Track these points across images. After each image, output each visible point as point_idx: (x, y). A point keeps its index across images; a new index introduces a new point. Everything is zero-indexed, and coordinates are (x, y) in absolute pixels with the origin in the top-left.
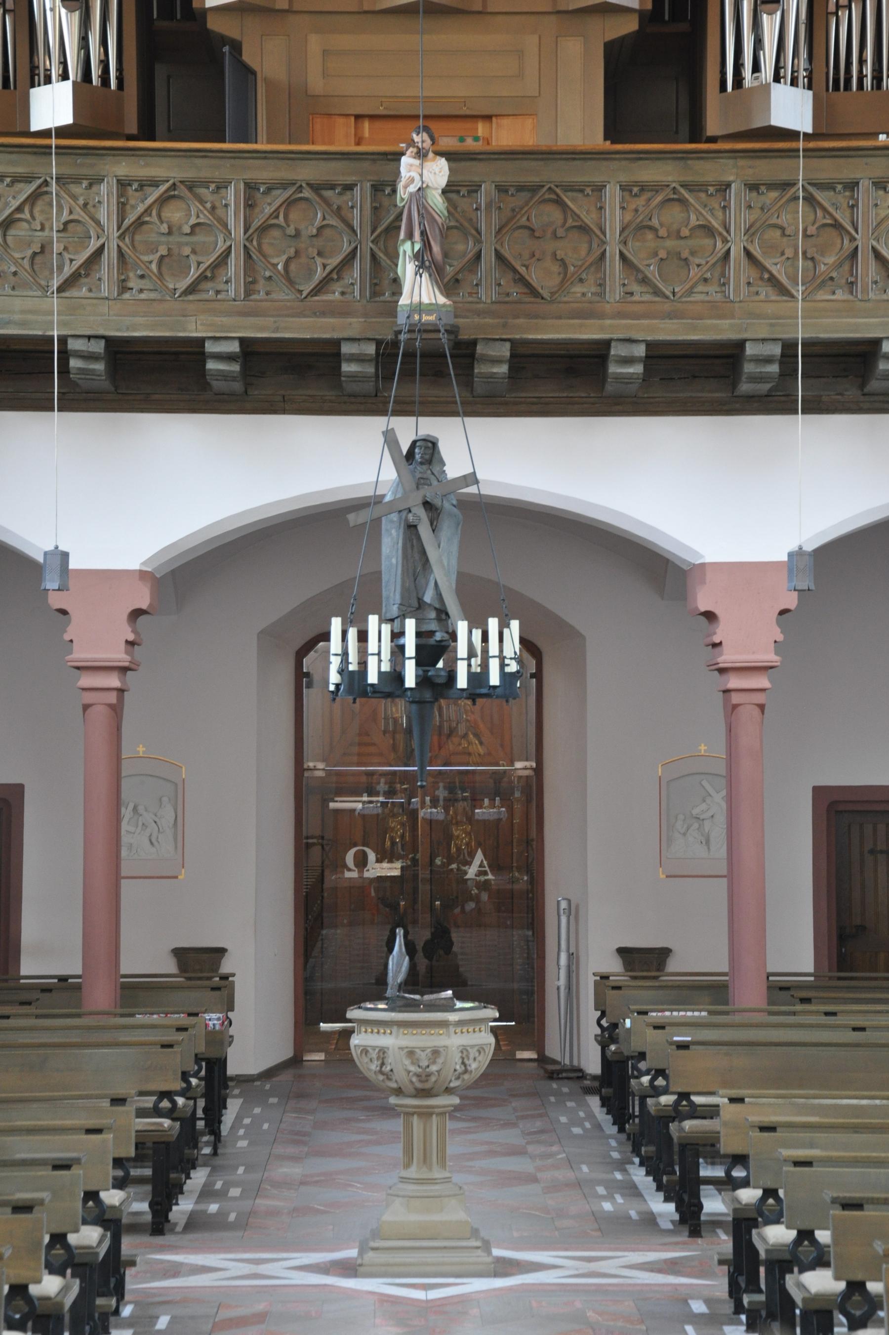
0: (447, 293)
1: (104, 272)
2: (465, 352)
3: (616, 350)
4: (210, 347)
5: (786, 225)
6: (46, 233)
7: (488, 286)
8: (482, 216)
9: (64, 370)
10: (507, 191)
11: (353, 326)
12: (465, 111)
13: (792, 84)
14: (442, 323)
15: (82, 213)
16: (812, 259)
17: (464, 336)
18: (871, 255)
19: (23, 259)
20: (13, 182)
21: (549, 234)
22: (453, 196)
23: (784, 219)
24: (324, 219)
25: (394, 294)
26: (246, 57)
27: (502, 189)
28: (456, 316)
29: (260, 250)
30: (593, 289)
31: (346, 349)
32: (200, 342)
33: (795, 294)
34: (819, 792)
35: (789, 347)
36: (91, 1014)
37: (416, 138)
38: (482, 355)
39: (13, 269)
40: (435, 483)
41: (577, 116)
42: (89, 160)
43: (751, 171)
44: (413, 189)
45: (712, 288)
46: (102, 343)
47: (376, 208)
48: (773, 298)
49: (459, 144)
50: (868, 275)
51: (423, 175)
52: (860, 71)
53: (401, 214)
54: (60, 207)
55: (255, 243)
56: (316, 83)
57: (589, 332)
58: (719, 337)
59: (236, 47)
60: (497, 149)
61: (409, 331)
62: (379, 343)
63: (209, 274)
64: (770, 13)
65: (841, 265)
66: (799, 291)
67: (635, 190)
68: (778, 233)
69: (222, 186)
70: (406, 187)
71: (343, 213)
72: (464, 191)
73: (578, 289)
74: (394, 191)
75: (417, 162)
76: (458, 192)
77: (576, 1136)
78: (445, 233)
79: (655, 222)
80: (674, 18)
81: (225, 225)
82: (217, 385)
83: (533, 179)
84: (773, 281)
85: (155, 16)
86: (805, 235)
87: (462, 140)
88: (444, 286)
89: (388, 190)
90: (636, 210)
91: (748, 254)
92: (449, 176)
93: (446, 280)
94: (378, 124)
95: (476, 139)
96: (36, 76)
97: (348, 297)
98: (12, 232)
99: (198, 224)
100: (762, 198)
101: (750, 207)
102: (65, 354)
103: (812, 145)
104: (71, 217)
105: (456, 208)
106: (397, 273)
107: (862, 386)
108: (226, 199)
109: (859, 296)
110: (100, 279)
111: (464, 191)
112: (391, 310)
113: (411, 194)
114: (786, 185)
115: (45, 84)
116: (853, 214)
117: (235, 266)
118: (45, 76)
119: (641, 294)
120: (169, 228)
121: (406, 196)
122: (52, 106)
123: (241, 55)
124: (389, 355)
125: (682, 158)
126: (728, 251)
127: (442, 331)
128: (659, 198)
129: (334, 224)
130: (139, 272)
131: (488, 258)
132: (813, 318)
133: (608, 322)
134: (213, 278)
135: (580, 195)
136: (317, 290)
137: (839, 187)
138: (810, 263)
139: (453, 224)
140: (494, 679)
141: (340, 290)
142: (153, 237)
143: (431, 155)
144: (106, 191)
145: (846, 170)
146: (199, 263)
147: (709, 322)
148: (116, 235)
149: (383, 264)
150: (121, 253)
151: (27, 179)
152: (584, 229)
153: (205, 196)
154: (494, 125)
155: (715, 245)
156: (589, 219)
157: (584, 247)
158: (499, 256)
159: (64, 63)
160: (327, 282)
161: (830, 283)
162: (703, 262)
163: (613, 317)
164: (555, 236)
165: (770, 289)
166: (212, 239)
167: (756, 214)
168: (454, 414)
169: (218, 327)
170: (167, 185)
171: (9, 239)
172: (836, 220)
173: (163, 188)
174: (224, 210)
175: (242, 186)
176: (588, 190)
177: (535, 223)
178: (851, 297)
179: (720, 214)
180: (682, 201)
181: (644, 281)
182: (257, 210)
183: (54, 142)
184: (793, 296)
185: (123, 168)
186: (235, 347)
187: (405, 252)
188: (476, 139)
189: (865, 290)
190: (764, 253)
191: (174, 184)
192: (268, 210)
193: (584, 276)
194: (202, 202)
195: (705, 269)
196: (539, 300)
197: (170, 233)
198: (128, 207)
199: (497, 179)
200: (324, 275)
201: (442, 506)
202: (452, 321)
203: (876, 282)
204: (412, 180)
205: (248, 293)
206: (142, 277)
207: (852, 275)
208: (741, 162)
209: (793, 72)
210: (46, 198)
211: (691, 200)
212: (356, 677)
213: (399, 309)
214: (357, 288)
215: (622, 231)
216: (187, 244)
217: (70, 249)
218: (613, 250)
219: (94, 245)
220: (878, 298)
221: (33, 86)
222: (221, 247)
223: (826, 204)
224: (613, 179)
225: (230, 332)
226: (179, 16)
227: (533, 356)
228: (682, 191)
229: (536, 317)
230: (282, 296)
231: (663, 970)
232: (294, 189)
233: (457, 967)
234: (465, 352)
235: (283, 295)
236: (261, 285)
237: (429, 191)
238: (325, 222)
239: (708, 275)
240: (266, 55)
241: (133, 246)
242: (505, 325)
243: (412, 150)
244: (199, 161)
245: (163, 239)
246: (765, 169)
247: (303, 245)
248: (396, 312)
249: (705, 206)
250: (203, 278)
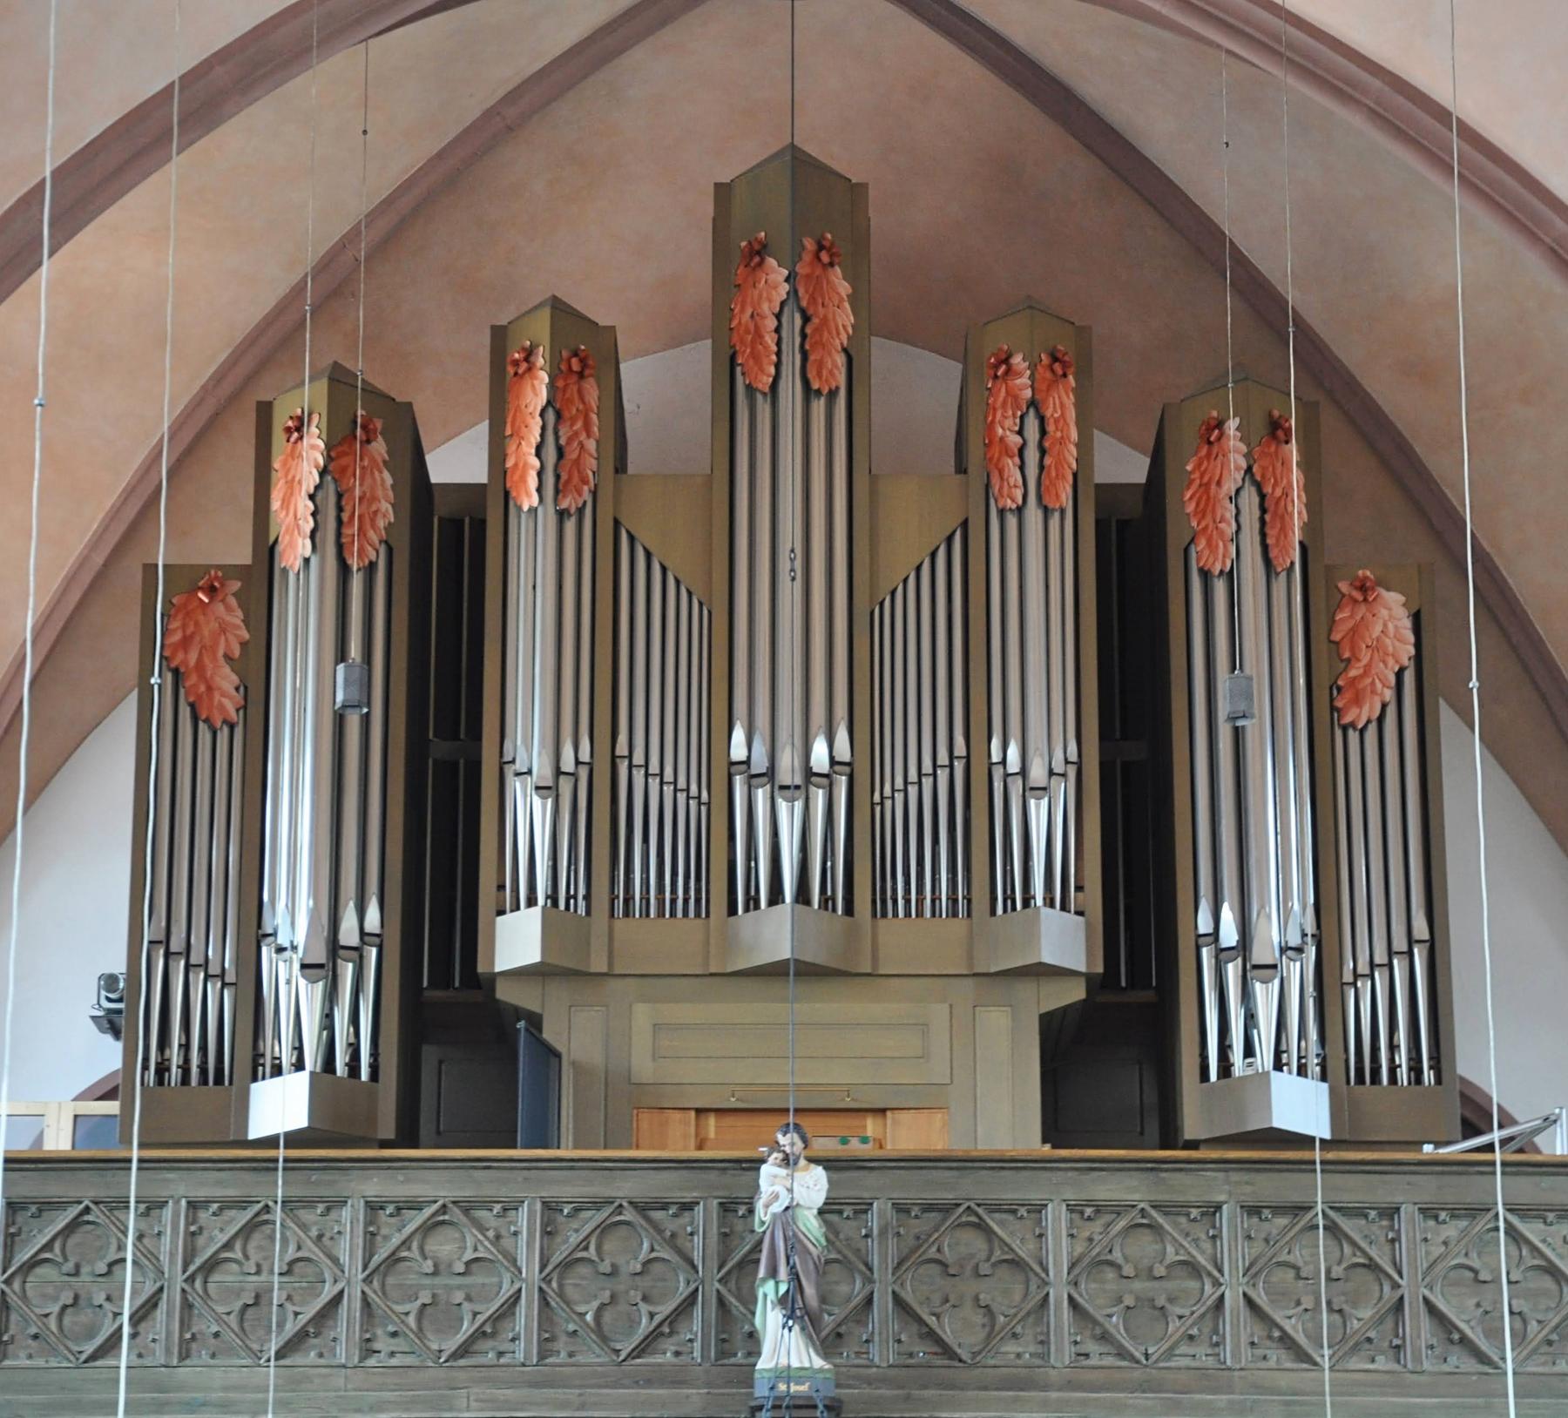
1: (342, 1329)
5: (1300, 1263)
6: (263, 1277)
7: (883, 1342)
8: (874, 1245)
10: (908, 1212)
12: (848, 1103)
13: (1299, 1074)
14: (821, 1394)
15: (316, 1250)
16: (1340, 1311)
19: (228, 1314)
20: (221, 1209)
21: (968, 1270)
22: (834, 1218)
23: (1297, 1257)
24: (652, 1250)
27: (901, 1209)
28: (838, 1386)
29: (561, 1294)
30: (1032, 1349)
33: (1318, 1359)
37: (783, 1140)
39: (214, 1328)
41: (1002, 1107)
43: (1248, 1189)
44: (777, 1208)
45: (1201, 1350)
47: (726, 1235)
48: (1289, 1365)
49: (840, 1147)
50: (1419, 1336)
51: (791, 1191)
52: (1392, 1060)
53: (760, 1242)
54: (285, 1240)
55: (554, 1285)
56: (643, 1066)
59: (535, 1021)
60: (894, 1155)
61: (775, 1407)
65: (1381, 1321)
67: (1089, 1211)
68: (1291, 1274)
69: (510, 1207)
70: (767, 1206)
71: (679, 1242)
72: (848, 1211)
73: (1011, 1348)
74: (751, 1211)
75: (783, 1172)
76: (840, 1212)
78: (823, 1268)
79: (1117, 1256)
80: (1132, 984)
81: (514, 1261)
84: (1286, 1341)
85: (425, 984)
86: (1329, 1279)
87: (845, 1141)
88: (823, 1342)
89: (742, 1211)
90: (1090, 1240)
91: (1250, 1302)
92: (829, 1191)
93: (824, 1334)
94: (729, 1121)
95: (864, 1140)
96: (259, 1066)
97: (684, 1359)
100: (1266, 1225)
101: (1249, 1237)
103: (1331, 1156)
104: (300, 1254)
105: (837, 1234)
106: (753, 1325)
108: (515, 1223)
109: (1410, 1366)
110: (335, 1340)
111: (848, 1211)
112: (746, 1376)
113: (774, 1215)
115: (272, 1076)
116: (1394, 1250)
117: (525, 1318)
118: (273, 1066)
119: (1098, 1355)
120: (435, 1265)
121: (767, 1219)
122: (280, 1105)
123: (540, 1031)
125: (1152, 1169)
127: (821, 1407)
128: (1122, 1223)
129: (666, 1256)
130: (391, 1328)
133: (1054, 1395)
134: (494, 1335)
135: (1010, 1217)
136: (640, 1350)
137: (1373, 1214)
138: (1337, 1317)
139: (833, 1256)
141: (673, 1348)
142: (412, 1279)
143: (802, 1162)
144: (350, 1217)
146: (475, 1314)
147: (1198, 1396)
148: (361, 1276)
149: (734, 1311)
150: (366, 1303)
151: (242, 1204)
152: (1016, 1263)
154: (889, 1121)
155: (1203, 1290)
156: (1024, 1251)
158: (898, 1301)
159: (299, 1049)
160: (655, 1339)
161: (1367, 1346)
162: (1187, 1312)
164: (977, 1274)
165: (1283, 1354)
166: (495, 1280)
167: (1258, 1247)
170: (435, 1207)
172: (1371, 1259)
173: (428, 1211)
174: (513, 1239)
175: (538, 1206)
176: (1023, 1211)
177: (948, 1255)
178: (1396, 1367)
179: (1207, 1246)
180: (1153, 1227)
181: (1105, 1337)
182: (559, 1239)
183: (281, 1153)
184: (1315, 1364)
185: (375, 1186)
187: (765, 1296)
188: (864, 1140)
189: (1417, 1359)
190: (1272, 1302)
191: (444, 1206)
192: (574, 1239)
193: (1018, 1329)
194: (483, 1230)
195: (1190, 1322)
196: (957, 1364)
197: (436, 1273)
198: (379, 1238)
199: (895, 1195)
202: (835, 1392)
203: (1432, 1347)
204: (776, 1197)
205: (542, 1356)
206: (394, 1334)
207: (1397, 1336)
208: (1235, 1177)
209: (1300, 1058)
210: (267, 1229)
211: (1167, 1227)
213: (757, 1375)
214: (697, 1345)
216: (459, 1287)
217: (296, 1298)
218: (1058, 1293)
220: (1436, 1369)
221: (255, 1079)
222: (507, 1290)
224: (1053, 1198)
225: (516, 1410)
226: (457, 984)
228: (1154, 1213)
229: (952, 1387)
230: (593, 1359)
232: (611, 1209)
235: (593, 1356)
236: (562, 1345)
237: (799, 1211)
238: (654, 1255)
239: (1194, 1331)
240: (575, 1032)
241: (384, 1293)
245: (427, 1281)
246: (1269, 1187)
247: (622, 1287)
248: (752, 1379)
249: (1187, 1235)
250: (480, 1334)
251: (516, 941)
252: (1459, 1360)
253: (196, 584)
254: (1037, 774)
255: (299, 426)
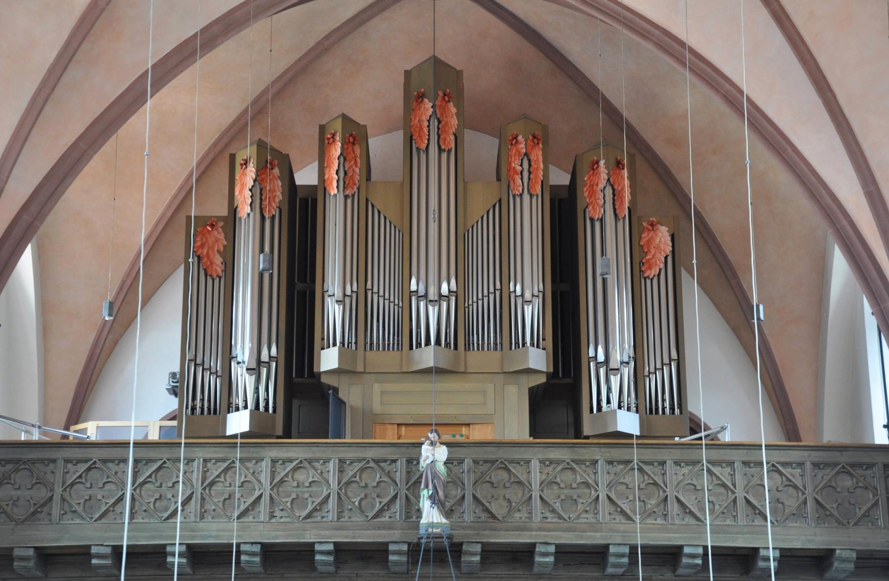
2: (457, 549)
4: (318, 547)
6: (232, 488)
7: (469, 513)
8: (465, 475)
9: (238, 562)
10: (478, 463)
11: (396, 535)
12: (456, 421)
16: (643, 501)
17: (455, 540)
18: (675, 500)
22: (450, 465)
23: (627, 480)
25: (418, 517)
26: (341, 395)
27: (476, 462)
28: (452, 529)
29: (346, 495)
31: (392, 547)
35: (633, 549)
41: (516, 425)
43: (608, 454)
44: (428, 461)
45: (590, 516)
46: (259, 546)
51: (433, 455)
52: (663, 405)
54: (240, 474)
56: (377, 408)
57: (524, 539)
58: (594, 542)
59: (336, 390)
60: (473, 441)
61: (428, 538)
62: (409, 544)
66: (637, 518)
67: (547, 463)
68: (624, 487)
69: (326, 461)
72: (455, 463)
73: (517, 515)
74: (418, 463)
75: (431, 448)
78: (446, 485)
79: (558, 480)
80: (564, 376)
81: (328, 482)
82: (320, 568)
84: (623, 512)
86: (639, 489)
87: (454, 436)
91: (609, 498)
94: (410, 428)
95: (462, 436)
96: (231, 407)
98: (214, 488)
99: (313, 481)
102: (239, 553)
103: (640, 442)
107: (674, 571)
111: (455, 463)
114: (628, 462)
117: (332, 503)
121: (425, 466)
122: (238, 423)
124: (416, 551)
126: (598, 496)
128: (560, 467)
131: (469, 498)
133: (534, 533)
134: (320, 510)
136: (376, 516)
142: (289, 489)
143: (438, 444)
144: (265, 465)
145: (660, 455)
150: (271, 498)
151: (223, 460)
152: (520, 483)
156: (523, 478)
158: (475, 497)
159: (246, 401)
164: (505, 487)
167: (612, 476)
171: (212, 492)
173: (295, 463)
176: (522, 463)
177: (494, 480)
179: (592, 476)
180: (572, 469)
181: (553, 511)
183: (239, 441)
185: (275, 453)
188: (462, 436)
189: (673, 519)
192: (351, 473)
194: (316, 470)
197: (298, 486)
202: (450, 532)
204: (428, 457)
205: (339, 518)
206: (282, 510)
208: (603, 450)
210: (233, 469)
214: (398, 514)
218: (536, 494)
219: (257, 493)
221: (229, 412)
222: (325, 493)
224: (535, 457)
229: (495, 530)
234: (457, 549)
235: (358, 518)
236: (346, 514)
239: (588, 509)
240: (351, 394)
242: (478, 534)
245: (295, 490)
246: (616, 454)
247: (368, 492)
251: (329, 360)
252: (689, 520)
253: (206, 223)
254: (528, 296)
255: (246, 163)
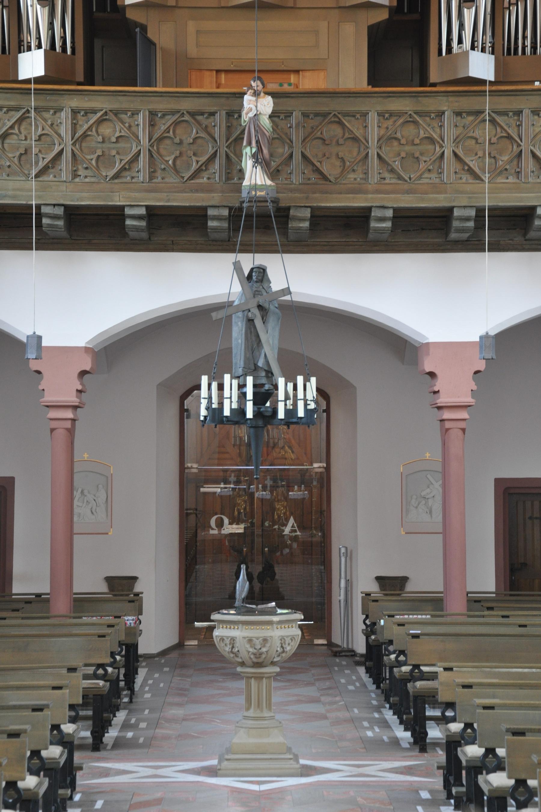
0: (272, 178)
1: (63, 165)
2: (283, 214)
3: (375, 213)
4: (128, 211)
5: (478, 137)
6: (28, 142)
7: (297, 174)
8: (294, 131)
9: (39, 225)
10: (308, 116)
11: (215, 198)
12: (283, 68)
13: (482, 51)
14: (269, 196)
15: (50, 130)
16: (494, 157)
17: (282, 204)
18: (530, 155)
19: (14, 157)
20: (8, 111)
21: (334, 143)
22: (276, 119)
23: (477, 133)
24: (197, 133)
25: (240, 179)
26: (150, 35)
27: (305, 115)
28: (277, 192)
29: (158, 152)
30: (361, 176)
31: (211, 212)
32: (122, 208)
33: (484, 179)
34: (498, 482)
35: (480, 211)
36: (55, 617)
37: (253, 84)
38: (293, 216)
39: (8, 164)
40: (265, 294)
41: (351, 71)
42: (54, 98)
43: (457, 104)
44: (251, 115)
45: (433, 175)
46: (62, 209)
47: (229, 127)
48: (471, 181)
49: (279, 88)
50: (528, 167)
51: (257, 107)
52: (524, 43)
53: (244, 130)
54: (37, 126)
55: (155, 148)
56: (192, 51)
57: (358, 202)
58: (437, 205)
59: (144, 28)
60: (302, 91)
61: (249, 201)
62: (230, 208)
63: (127, 167)
64: (469, 8)
65: (512, 161)
66: (486, 177)
67: (387, 115)
68: (474, 141)
69: (135, 113)
70: (247, 114)
71: (209, 129)
72: (282, 116)
73: (352, 176)
74: (240, 116)
75: (254, 99)
76: (279, 117)
77: (351, 691)
78: (271, 142)
79: (399, 135)
80: (410, 11)
81: (137, 137)
82: (132, 234)
83: (325, 109)
84: (470, 171)
85: (94, 10)
86: (490, 143)
87: (281, 85)
88: (270, 174)
89: (236, 116)
90: (387, 128)
91: (455, 154)
92: (273, 107)
93: (271, 170)
94: (230, 76)
95: (290, 85)
96: (22, 46)
97: (212, 181)
98: (7, 141)
99: (121, 136)
100: (464, 120)
101: (456, 126)
102: (39, 216)
103: (494, 88)
104: (44, 132)
105: (277, 126)
106: (241, 166)
107: (525, 235)
108: (137, 121)
109: (523, 180)
110: (61, 170)
111: (282, 116)
112: (238, 188)
113: (250, 118)
114: (479, 113)
115: (28, 51)
116: (519, 130)
117: (143, 162)
118: (28, 46)
119: (390, 179)
120: (103, 138)
121: (247, 120)
122: (32, 65)
123: (146, 33)
124: (237, 216)
125: (415, 96)
126: (443, 153)
127: (269, 201)
128: (401, 121)
129: (203, 136)
130: (85, 166)
131: (297, 157)
132: (495, 193)
133: (370, 196)
134: (129, 169)
135: (353, 119)
136: (193, 177)
137: (511, 114)
138: (493, 160)
139: (275, 136)
140: (301, 413)
141: (207, 176)
142: (93, 144)
143: (262, 94)
144: (65, 116)
145: (515, 103)
146: (121, 160)
147: (431, 196)
148: (71, 143)
149: (233, 160)
150: (74, 154)
151: (17, 109)
152: (355, 139)
153: (125, 119)
154: (301, 76)
155: (435, 149)
156: (358, 133)
157: (355, 151)
158: (304, 156)
159: (39, 39)
160: (199, 172)
161: (505, 172)
162: (428, 160)
163: (373, 193)
164: (338, 144)
165: (468, 176)
166: (129, 145)
167: (460, 130)
168: (276, 252)
169: (133, 199)
170: (102, 113)
171: (6, 145)
172: (509, 134)
173: (99, 114)
174: (136, 127)
175: (147, 113)
176: (358, 116)
177: (325, 135)
178: (518, 181)
179: (438, 130)
180: (415, 122)
181: (392, 171)
182: (156, 128)
183: (33, 86)
184: (482, 180)
185: (75, 102)
186: (143, 211)
187: (246, 153)
188: (290, 85)
189: (526, 177)
190: (465, 154)
191: (106, 112)
192: (163, 128)
193: (355, 168)
194: (123, 123)
195: (429, 164)
196: (328, 183)
197: (103, 142)
198: (78, 126)
199: (303, 109)
200: (197, 167)
201: (269, 308)
202: (275, 195)
203: (533, 172)
204: (251, 110)
205: (151, 178)
206: (86, 168)
207: (518, 167)
208: (451, 99)
209: (482, 44)
210: (28, 120)
211: (420, 122)
212: (217, 412)
213: (243, 188)
214: (217, 175)
215: (379, 140)
216: (114, 148)
217: (43, 151)
218: (373, 152)
219: (57, 149)
220: (534, 181)
221: (20, 52)
222: (135, 150)
223: (503, 124)
224: (373, 109)
225: (140, 202)
226: (109, 10)
227: (324, 216)
228: (415, 116)
229: (326, 193)
230: (172, 180)
231: (403, 590)
232: (179, 115)
233: (278, 588)
234: (283, 214)
235: (172, 179)
236: (159, 174)
237: (261, 116)
238: (198, 135)
239: (431, 167)
240: (162, 34)
241: (81, 150)
242: (307, 198)
243: (250, 91)
244: (121, 98)
245: (99, 145)
246: (466, 103)
247: (184, 149)
248: (241, 189)
249: (429, 125)
250: (123, 169)
